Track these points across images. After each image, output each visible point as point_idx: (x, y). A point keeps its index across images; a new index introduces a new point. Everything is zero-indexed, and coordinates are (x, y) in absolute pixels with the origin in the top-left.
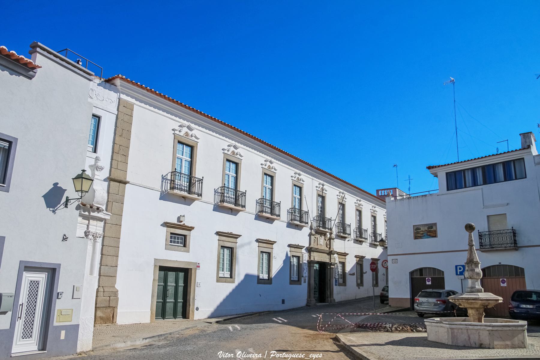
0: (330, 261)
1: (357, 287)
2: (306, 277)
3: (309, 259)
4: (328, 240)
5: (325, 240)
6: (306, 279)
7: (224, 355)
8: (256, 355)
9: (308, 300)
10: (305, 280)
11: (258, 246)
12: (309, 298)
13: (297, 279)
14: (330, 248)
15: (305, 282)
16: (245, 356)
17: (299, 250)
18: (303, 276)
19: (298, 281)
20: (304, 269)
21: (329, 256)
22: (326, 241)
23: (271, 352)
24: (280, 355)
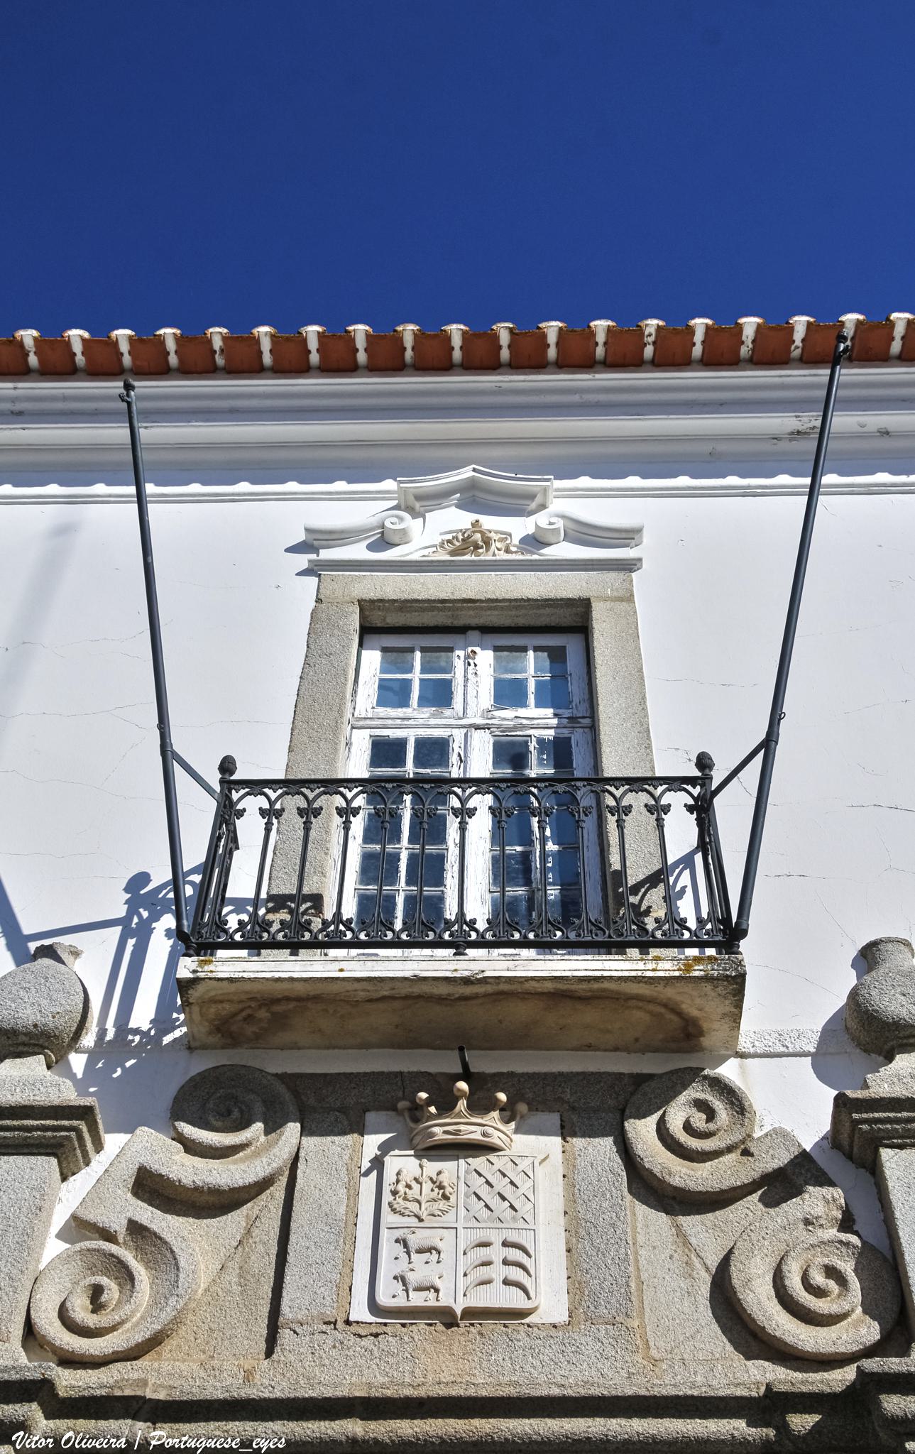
7: (29, 1440)
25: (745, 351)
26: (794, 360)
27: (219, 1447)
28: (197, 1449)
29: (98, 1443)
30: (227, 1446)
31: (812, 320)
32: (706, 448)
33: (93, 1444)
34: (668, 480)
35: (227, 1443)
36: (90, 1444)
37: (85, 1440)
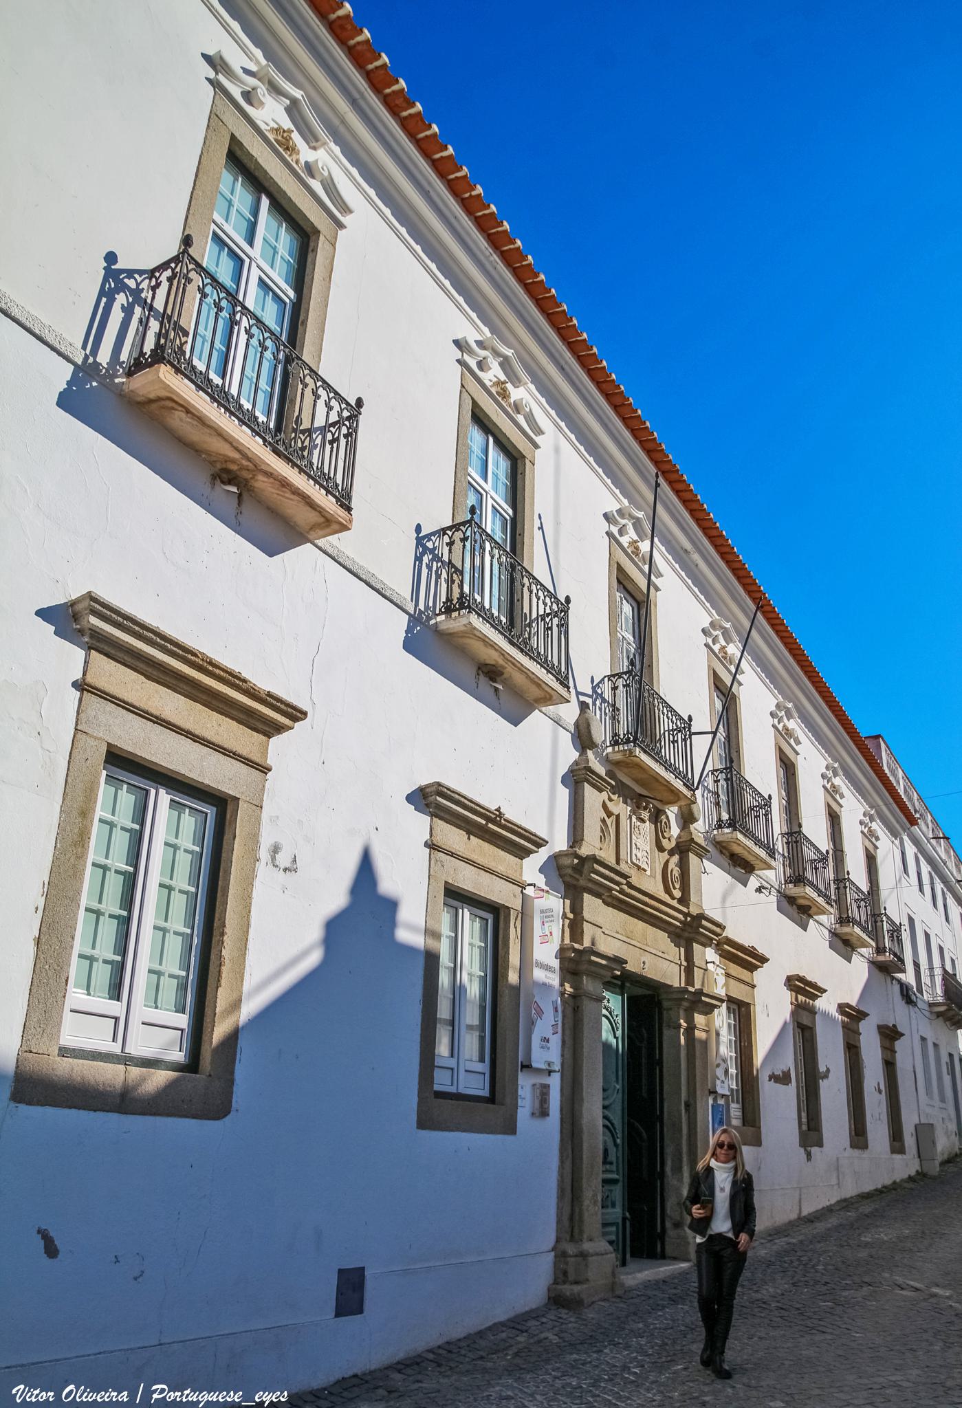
0: (690, 979)
1: (802, 1150)
2: (550, 1072)
3: (567, 941)
4: (671, 853)
5: (661, 849)
6: (547, 1087)
7: (30, 1394)
8: (113, 1394)
9: (560, 1255)
10: (543, 1093)
11: (81, 686)
12: (572, 1239)
13: (478, 1086)
14: (684, 900)
15: (543, 1113)
16: (86, 1397)
17: (503, 860)
18: (527, 1066)
19: (491, 1099)
20: (540, 1012)
21: (682, 950)
22: (665, 855)
23: (154, 1387)
24: (177, 1394)
25: (333, 16)
26: (328, 20)
27: (221, 1400)
28: (199, 1402)
29: (99, 1396)
30: (229, 1400)
31: (352, 14)
32: (670, 538)
33: (94, 1398)
34: (244, 35)
35: (230, 1397)
36: (91, 1397)
37: (86, 1394)
